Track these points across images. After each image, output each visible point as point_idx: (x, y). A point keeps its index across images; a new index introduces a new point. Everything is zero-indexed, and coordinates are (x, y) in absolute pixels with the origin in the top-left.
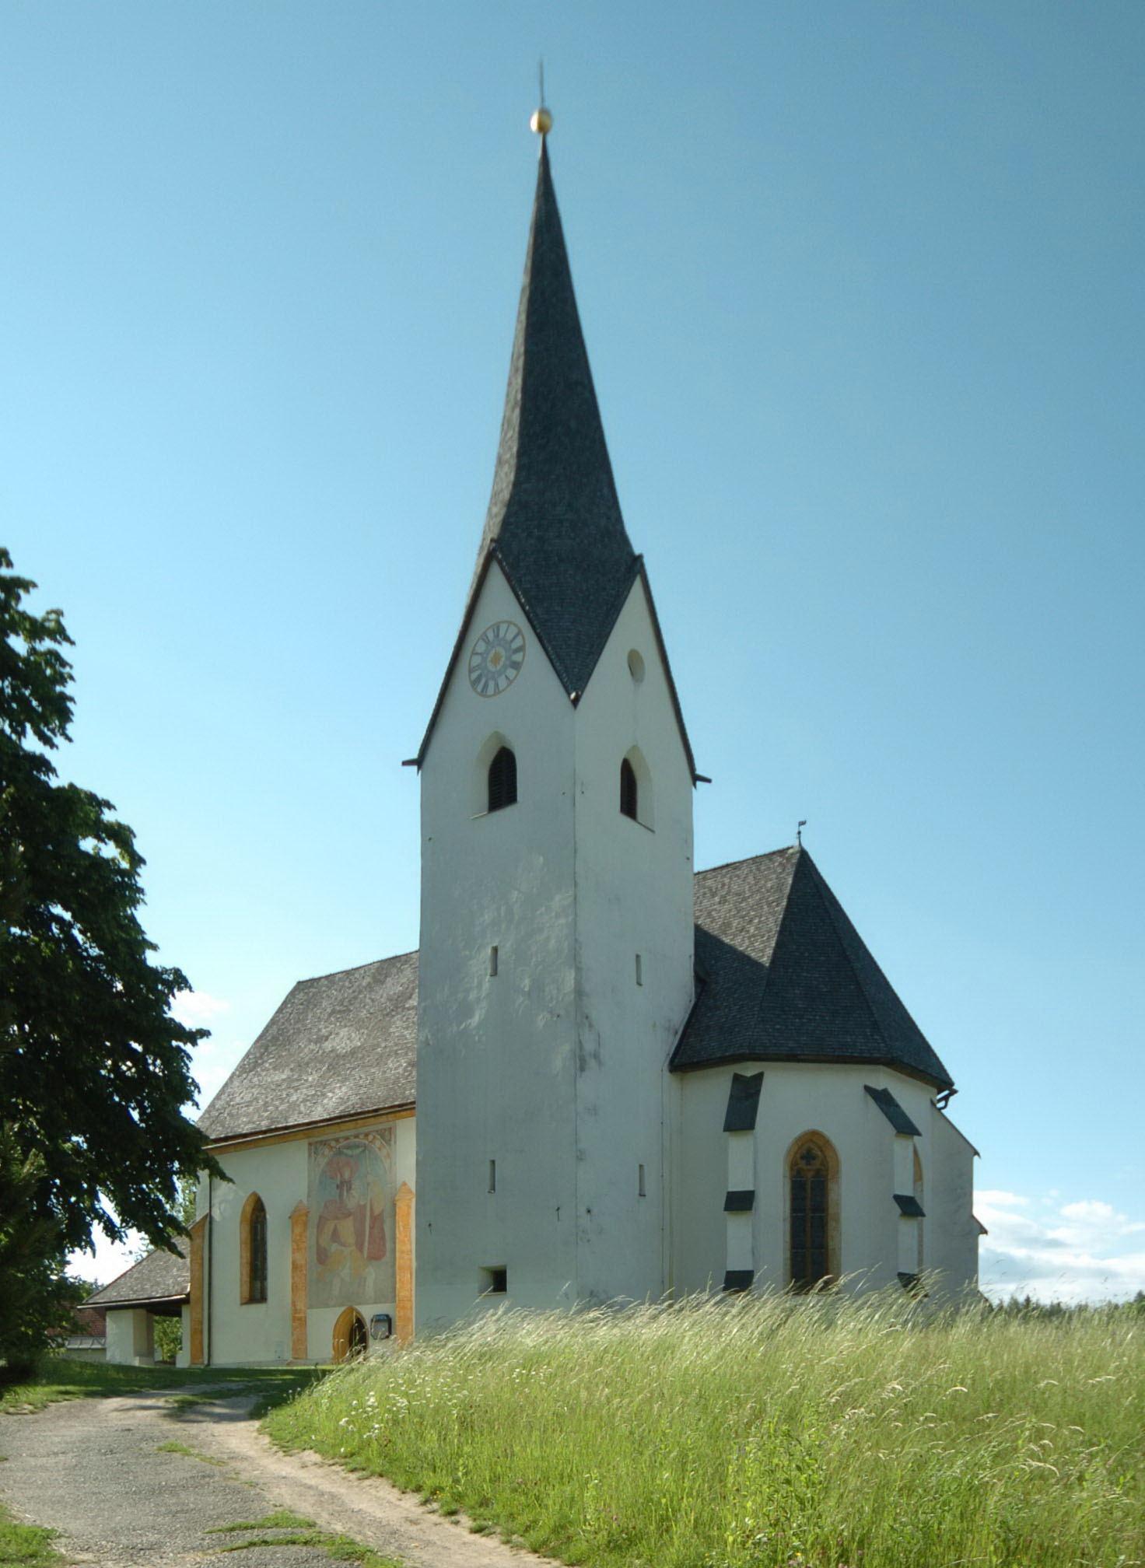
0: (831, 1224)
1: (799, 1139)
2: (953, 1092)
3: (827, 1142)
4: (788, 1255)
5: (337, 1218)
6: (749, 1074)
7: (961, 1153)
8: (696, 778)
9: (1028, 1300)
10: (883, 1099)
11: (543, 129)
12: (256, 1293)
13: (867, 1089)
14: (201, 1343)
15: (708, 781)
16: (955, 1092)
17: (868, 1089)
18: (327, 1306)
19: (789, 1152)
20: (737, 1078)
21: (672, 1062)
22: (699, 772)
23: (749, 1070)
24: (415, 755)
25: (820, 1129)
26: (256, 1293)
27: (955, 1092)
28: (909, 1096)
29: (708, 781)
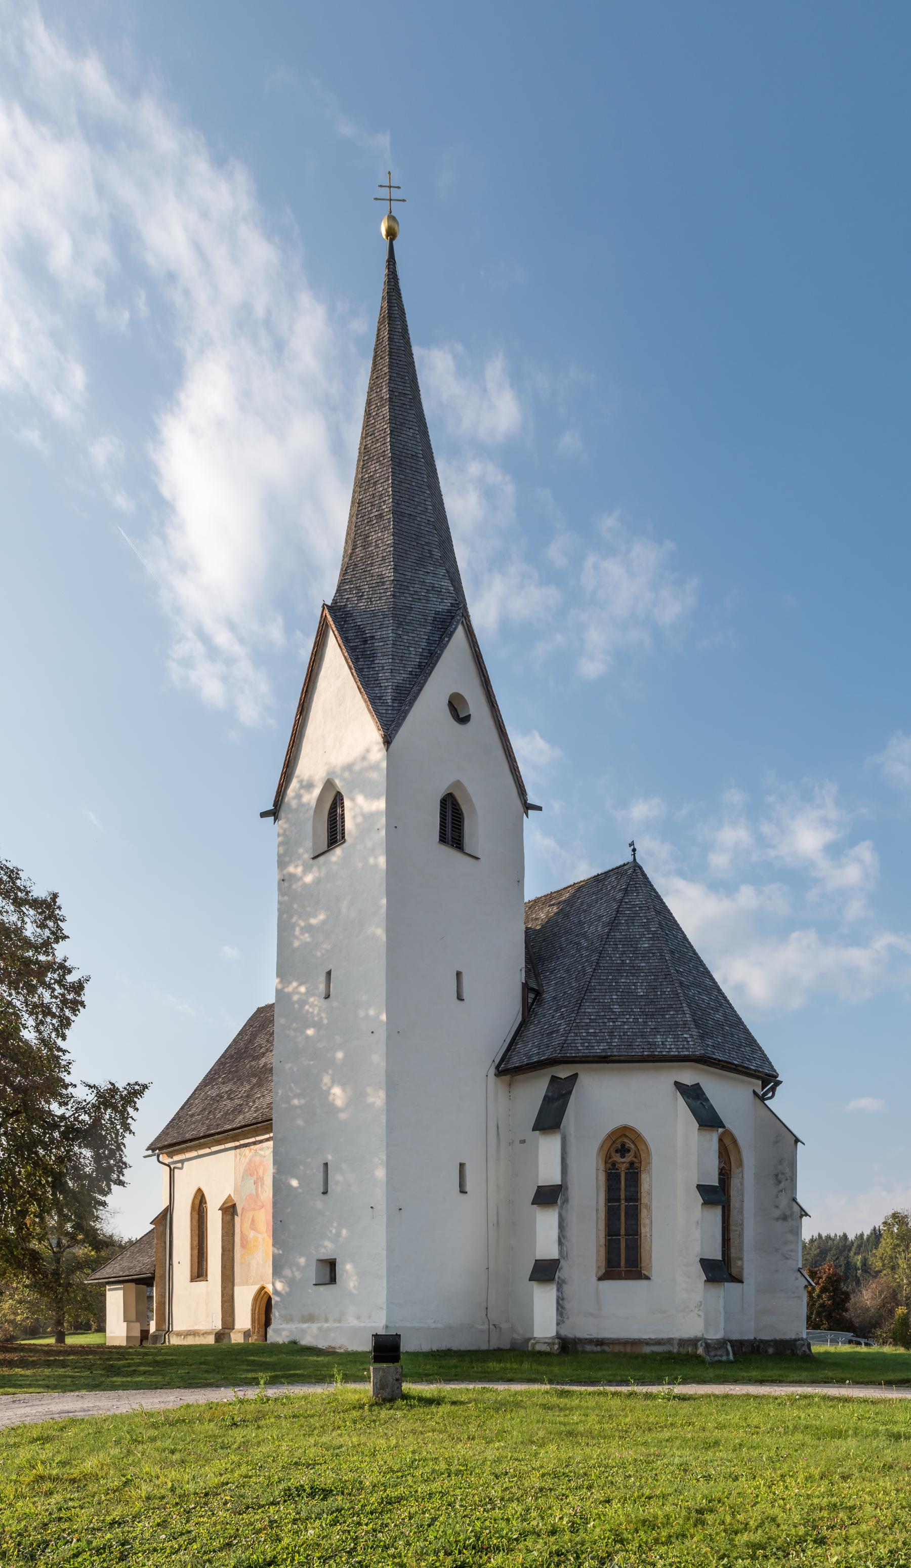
0: (644, 1213)
1: (610, 1136)
2: (778, 1083)
3: (639, 1136)
4: (602, 1241)
5: (254, 1210)
6: (563, 1075)
7: (783, 1144)
8: (529, 808)
9: (820, 1235)
10: (693, 1095)
11: (392, 234)
12: (199, 1273)
13: (677, 1084)
14: (164, 1314)
15: (539, 808)
16: (780, 1082)
17: (677, 1084)
18: (247, 1284)
19: (602, 1147)
20: (554, 1079)
21: (497, 1067)
22: (532, 799)
23: (563, 1072)
24: (270, 807)
25: (631, 1124)
26: (199, 1273)
27: (780, 1082)
28: (728, 1095)
29: (539, 808)
